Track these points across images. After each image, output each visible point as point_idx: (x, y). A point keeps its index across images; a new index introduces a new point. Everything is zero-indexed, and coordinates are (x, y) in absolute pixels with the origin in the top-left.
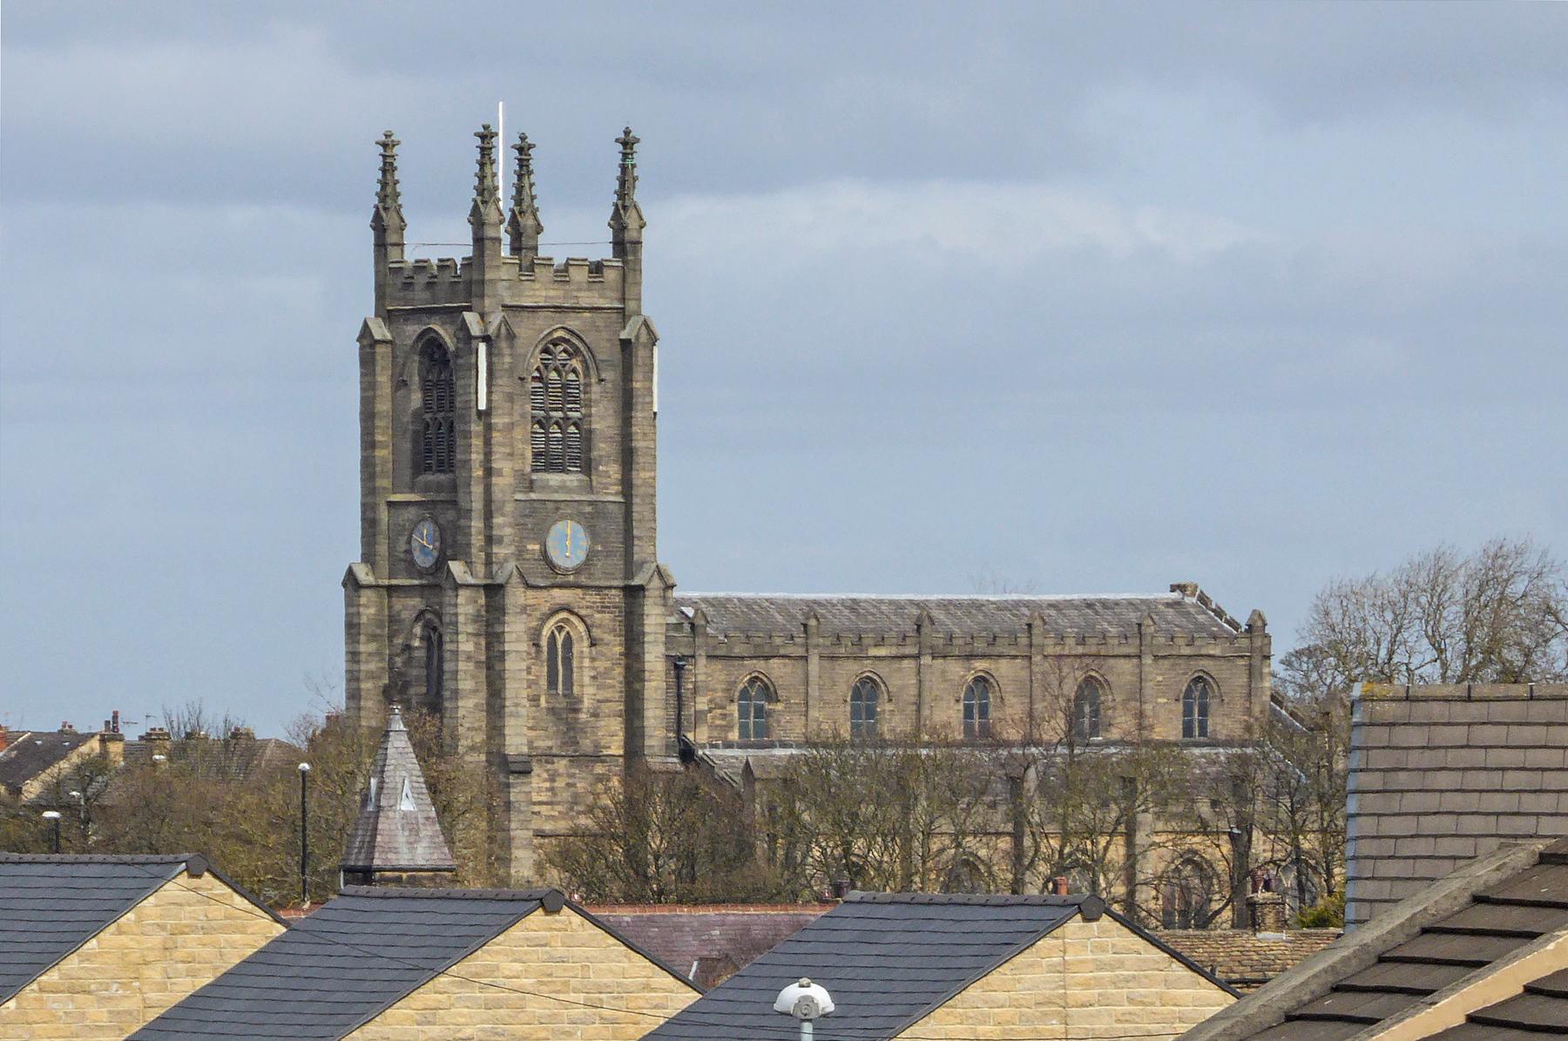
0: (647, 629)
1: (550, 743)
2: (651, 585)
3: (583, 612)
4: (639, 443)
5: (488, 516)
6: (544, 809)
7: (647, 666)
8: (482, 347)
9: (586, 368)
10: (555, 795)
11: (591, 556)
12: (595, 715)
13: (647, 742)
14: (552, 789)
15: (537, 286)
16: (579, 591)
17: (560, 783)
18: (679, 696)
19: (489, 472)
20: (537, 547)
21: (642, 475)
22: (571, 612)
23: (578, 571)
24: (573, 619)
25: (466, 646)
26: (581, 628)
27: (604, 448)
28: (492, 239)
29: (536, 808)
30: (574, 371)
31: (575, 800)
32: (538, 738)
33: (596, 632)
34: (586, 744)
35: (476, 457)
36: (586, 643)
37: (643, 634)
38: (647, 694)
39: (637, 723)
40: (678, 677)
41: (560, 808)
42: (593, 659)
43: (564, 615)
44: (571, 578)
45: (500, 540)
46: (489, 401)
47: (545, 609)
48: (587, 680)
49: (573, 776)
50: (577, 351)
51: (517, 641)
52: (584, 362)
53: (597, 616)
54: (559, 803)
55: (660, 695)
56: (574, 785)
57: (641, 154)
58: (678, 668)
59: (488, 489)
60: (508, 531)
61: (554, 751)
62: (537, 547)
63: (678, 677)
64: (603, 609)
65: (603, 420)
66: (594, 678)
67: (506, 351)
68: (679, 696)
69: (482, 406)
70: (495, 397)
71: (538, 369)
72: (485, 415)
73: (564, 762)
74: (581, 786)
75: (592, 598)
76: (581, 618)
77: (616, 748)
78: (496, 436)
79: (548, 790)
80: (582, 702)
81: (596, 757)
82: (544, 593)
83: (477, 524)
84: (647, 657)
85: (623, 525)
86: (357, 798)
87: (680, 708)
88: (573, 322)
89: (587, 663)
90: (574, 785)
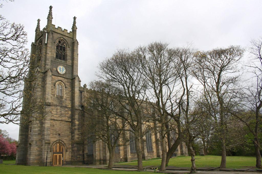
0: (75, 85)
1: (57, 103)
2: (76, 78)
3: (64, 82)
4: (75, 57)
5: (45, 61)
6: (55, 115)
7: (75, 91)
8: (47, 34)
9: (67, 45)
10: (57, 113)
11: (66, 73)
12: (66, 100)
13: (75, 104)
14: (57, 112)
15: (58, 30)
16: (63, 78)
17: (58, 111)
18: (81, 97)
19: (46, 53)
20: (56, 69)
21: (75, 62)
22: (62, 81)
23: (63, 75)
24: (62, 83)
25: (77, 123)
26: (64, 84)
27: (69, 58)
28: (50, 20)
29: (53, 115)
30: (64, 46)
31: (61, 114)
32: (54, 102)
33: (66, 86)
34: (64, 105)
35: (84, 167)
36: (64, 87)
37: (75, 86)
38: (75, 96)
39: (74, 101)
40: (81, 94)
41: (58, 115)
42: (66, 90)
43: (60, 82)
44: (62, 76)
45: (48, 65)
46: (47, 42)
47: (57, 80)
48: (64, 93)
49: (61, 110)
50: (65, 43)
51: (49, 81)
52: (66, 44)
53: (67, 83)
54: (58, 114)
55: (78, 96)
56: (61, 111)
57: (77, 20)
58: (81, 92)
59: (46, 56)
60: (50, 64)
61: (58, 105)
62: (56, 69)
63: (81, 94)
64: (68, 82)
65: (64, 118)
66: (66, 93)
67: (51, 35)
68: (81, 97)
69: (46, 43)
70: (48, 41)
71: (58, 43)
72: (46, 44)
73: (59, 107)
74: (63, 112)
75: (66, 80)
76: (64, 83)
77: (70, 106)
78: (48, 48)
79: (56, 112)
80: (63, 97)
81: (66, 107)
82: (56, 77)
83: (43, 62)
84: (75, 89)
85: (72, 68)
86: (205, 101)
87: (81, 99)
88: (64, 37)
89: (64, 90)
90: (61, 111)
